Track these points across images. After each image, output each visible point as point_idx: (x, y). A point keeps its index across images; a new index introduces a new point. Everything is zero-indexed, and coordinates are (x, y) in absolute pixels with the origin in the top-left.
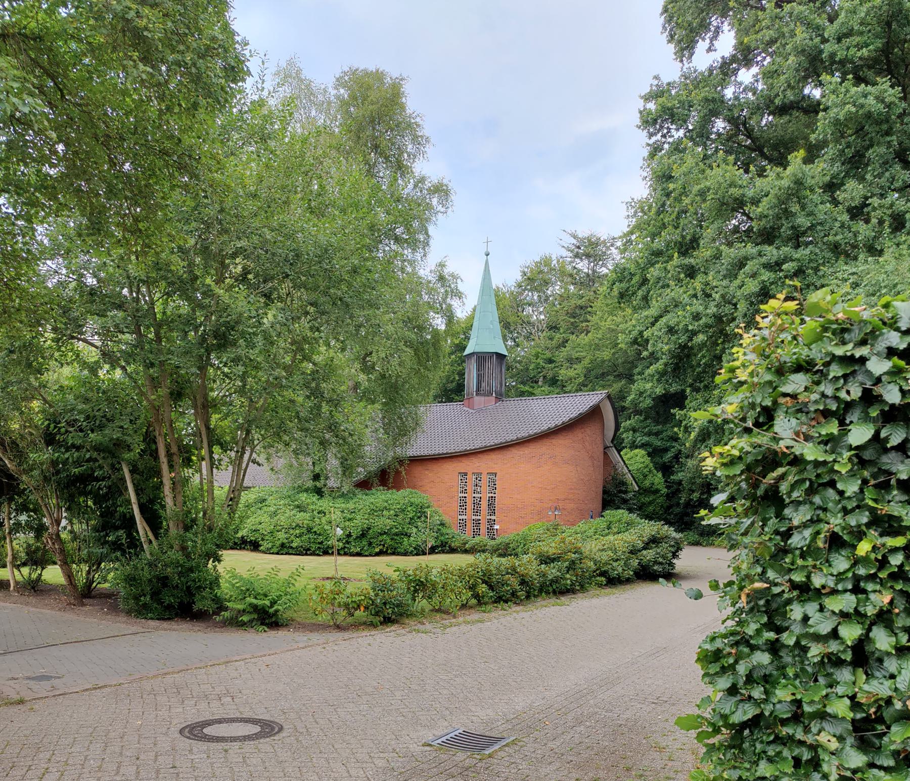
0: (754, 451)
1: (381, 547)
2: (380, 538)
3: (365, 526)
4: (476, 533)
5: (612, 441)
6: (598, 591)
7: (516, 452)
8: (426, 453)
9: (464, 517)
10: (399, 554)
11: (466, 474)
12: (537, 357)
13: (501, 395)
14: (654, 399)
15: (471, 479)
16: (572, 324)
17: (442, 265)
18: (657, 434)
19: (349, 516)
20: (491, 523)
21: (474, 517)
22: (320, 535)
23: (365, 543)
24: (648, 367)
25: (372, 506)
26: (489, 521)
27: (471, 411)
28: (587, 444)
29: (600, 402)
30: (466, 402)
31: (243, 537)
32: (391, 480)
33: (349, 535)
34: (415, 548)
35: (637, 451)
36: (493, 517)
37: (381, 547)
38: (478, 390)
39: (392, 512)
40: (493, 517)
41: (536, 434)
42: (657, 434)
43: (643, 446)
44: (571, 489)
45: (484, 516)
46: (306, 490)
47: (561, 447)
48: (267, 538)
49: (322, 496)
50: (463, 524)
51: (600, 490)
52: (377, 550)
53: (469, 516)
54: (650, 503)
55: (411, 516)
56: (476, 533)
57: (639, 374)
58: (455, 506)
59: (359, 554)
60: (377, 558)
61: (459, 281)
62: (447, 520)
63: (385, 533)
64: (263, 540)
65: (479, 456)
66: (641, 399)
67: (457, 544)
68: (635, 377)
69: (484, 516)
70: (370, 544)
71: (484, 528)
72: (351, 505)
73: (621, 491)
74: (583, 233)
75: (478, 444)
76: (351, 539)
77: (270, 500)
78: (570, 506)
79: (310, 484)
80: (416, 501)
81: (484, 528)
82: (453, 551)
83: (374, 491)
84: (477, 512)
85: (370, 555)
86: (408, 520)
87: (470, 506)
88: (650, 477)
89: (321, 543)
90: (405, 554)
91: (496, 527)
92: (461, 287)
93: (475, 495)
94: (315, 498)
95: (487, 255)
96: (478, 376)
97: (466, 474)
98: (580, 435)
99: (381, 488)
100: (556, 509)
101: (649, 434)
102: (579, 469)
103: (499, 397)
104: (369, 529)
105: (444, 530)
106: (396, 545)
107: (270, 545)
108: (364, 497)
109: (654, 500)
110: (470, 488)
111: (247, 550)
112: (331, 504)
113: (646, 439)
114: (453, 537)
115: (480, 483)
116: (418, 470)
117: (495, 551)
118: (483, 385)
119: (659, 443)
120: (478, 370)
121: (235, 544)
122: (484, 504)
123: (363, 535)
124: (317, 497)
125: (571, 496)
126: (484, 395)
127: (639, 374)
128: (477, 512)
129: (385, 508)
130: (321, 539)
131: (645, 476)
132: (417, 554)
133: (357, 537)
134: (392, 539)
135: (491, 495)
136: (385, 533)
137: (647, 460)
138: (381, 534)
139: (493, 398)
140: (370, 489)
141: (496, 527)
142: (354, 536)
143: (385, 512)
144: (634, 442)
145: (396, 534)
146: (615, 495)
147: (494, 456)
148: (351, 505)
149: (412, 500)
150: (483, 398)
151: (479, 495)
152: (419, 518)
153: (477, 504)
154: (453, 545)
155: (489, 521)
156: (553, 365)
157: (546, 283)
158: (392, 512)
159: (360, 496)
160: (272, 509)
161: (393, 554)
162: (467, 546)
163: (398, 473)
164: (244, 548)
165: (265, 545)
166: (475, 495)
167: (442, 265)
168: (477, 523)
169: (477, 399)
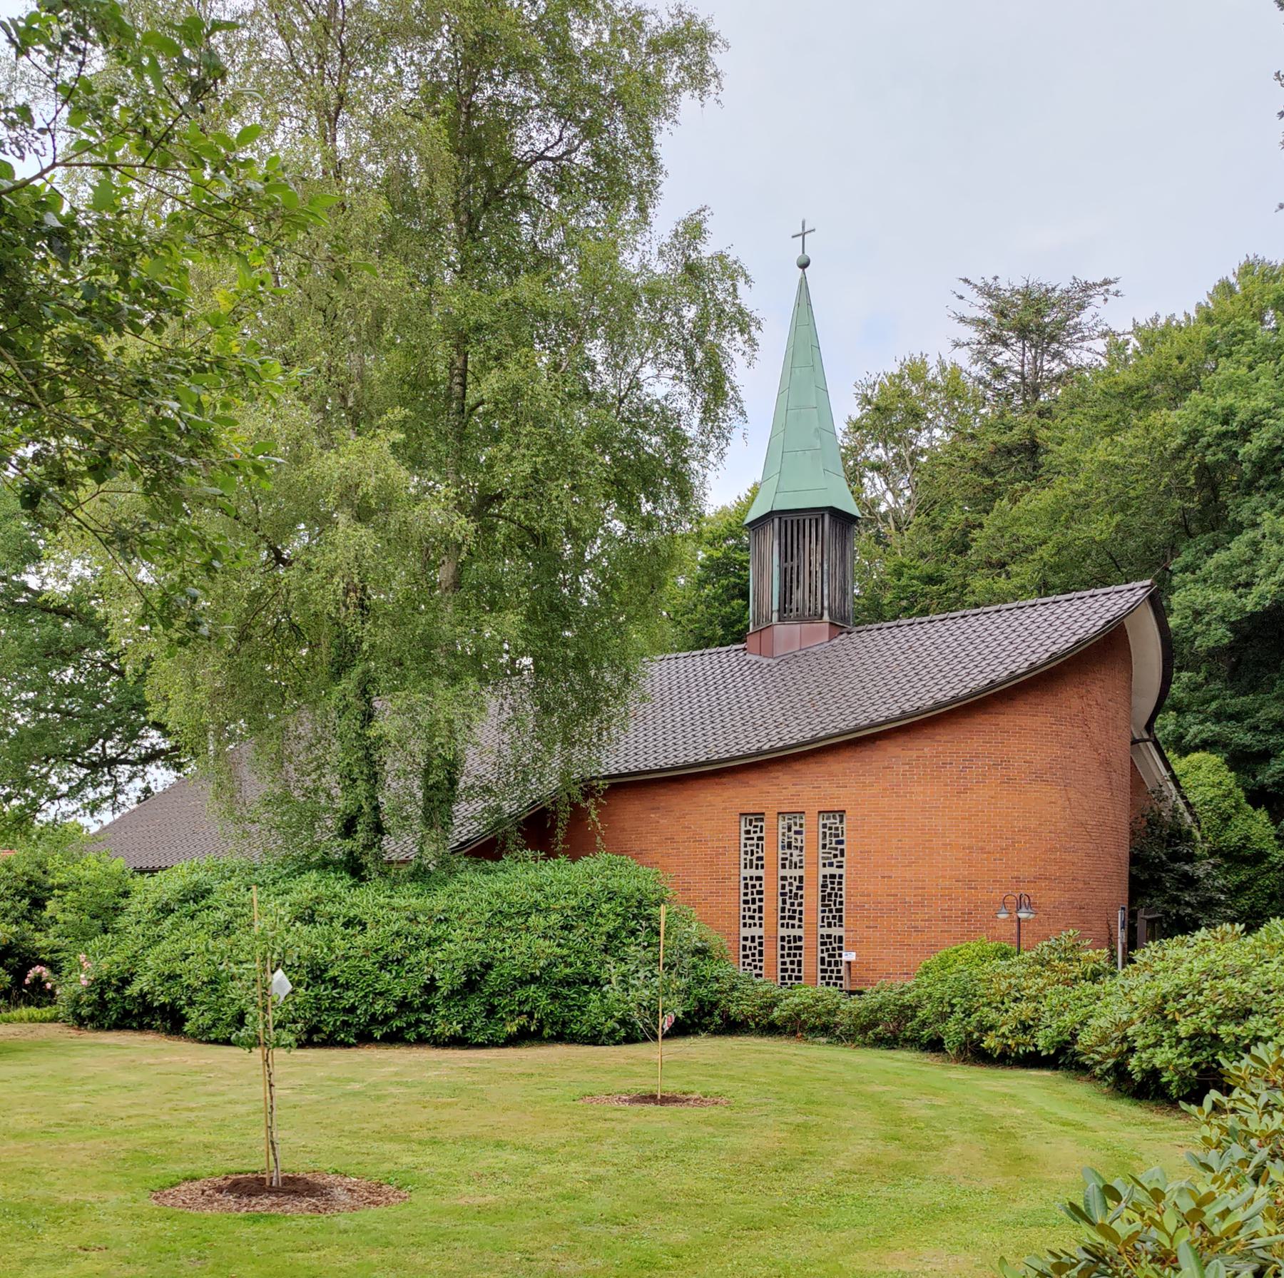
1: (523, 1020)
2: (520, 994)
3: (476, 959)
4: (791, 975)
7: (896, 755)
8: (651, 765)
9: (756, 931)
10: (574, 1039)
11: (760, 816)
12: (899, 574)
13: (844, 619)
14: (1234, 627)
15: (775, 829)
16: (986, 489)
17: (693, 230)
18: (1237, 717)
19: (429, 931)
20: (832, 946)
21: (783, 932)
22: (347, 987)
23: (475, 1006)
24: (1209, 553)
25: (497, 903)
26: (825, 940)
27: (765, 661)
28: (1094, 726)
29: (1131, 610)
30: (752, 641)
31: (143, 995)
32: (560, 835)
33: (431, 987)
34: (622, 1022)
35: (1196, 757)
36: (835, 931)
37: (523, 1020)
38: (785, 612)
39: (554, 918)
40: (835, 931)
41: (955, 699)
42: (1237, 717)
43: (1206, 745)
45: (812, 927)
46: (324, 865)
47: (1071, 700)
48: (199, 997)
49: (363, 879)
50: (753, 951)
51: (1125, 854)
52: (512, 1028)
53: (770, 928)
55: (609, 927)
56: (791, 975)
57: (1185, 569)
58: (733, 902)
59: (458, 1042)
60: (510, 1053)
61: (741, 283)
62: (715, 939)
63: (534, 979)
64: (191, 1003)
65: (797, 766)
66: (1198, 628)
67: (746, 1008)
68: (1176, 580)
69: (812, 927)
70: (491, 1011)
71: (811, 960)
72: (439, 901)
73: (1175, 857)
74: (1012, 278)
75: (795, 733)
76: (436, 999)
77: (222, 892)
78: (1049, 897)
79: (339, 849)
80: (627, 885)
81: (811, 960)
82: (732, 1027)
83: (507, 861)
84: (792, 916)
85: (491, 1044)
86: (600, 941)
87: (771, 903)
88: (1238, 821)
89: (352, 1010)
90: (594, 1039)
91: (849, 956)
92: (748, 298)
93: (787, 872)
94: (339, 884)
95: (804, 265)
96: (784, 573)
97: (760, 816)
98: (1076, 702)
99: (529, 853)
101: (1219, 717)
102: (1072, 795)
103: (840, 625)
104: (489, 967)
105: (708, 969)
106: (567, 1014)
107: (207, 1019)
108: (479, 879)
109: (1252, 880)
110: (773, 853)
111: (157, 1030)
112: (382, 900)
113: (1211, 729)
114: (734, 988)
115: (797, 841)
116: (632, 811)
117: (864, 1029)
118: (797, 595)
119: (1247, 739)
120: (786, 555)
121: (127, 1014)
122: (811, 898)
123: (471, 985)
124: (348, 881)
126: (801, 619)
127: (1185, 569)
128: (792, 916)
129: (536, 905)
130: (350, 997)
131: (1226, 819)
132: (630, 1040)
133: (453, 992)
134: (554, 997)
135: (828, 871)
136: (534, 979)
137: (1229, 778)
138: (523, 983)
139: (824, 626)
140: (498, 858)
141: (849, 956)
142: (445, 990)
143: (533, 919)
144: (1182, 737)
145: (567, 982)
146: (1161, 866)
147: (836, 766)
148: (439, 901)
149: (614, 884)
150: (797, 628)
151: (797, 873)
152: (633, 933)
153: (791, 895)
154: (734, 1009)
155: (825, 940)
156: (943, 587)
157: (916, 416)
158: (554, 918)
159: (466, 877)
160: (220, 916)
161: (559, 1038)
162: (776, 1013)
163: (578, 814)
164: (150, 1027)
165: (196, 1018)
166: (787, 872)
167: (693, 230)
168: (793, 946)
169: (782, 631)
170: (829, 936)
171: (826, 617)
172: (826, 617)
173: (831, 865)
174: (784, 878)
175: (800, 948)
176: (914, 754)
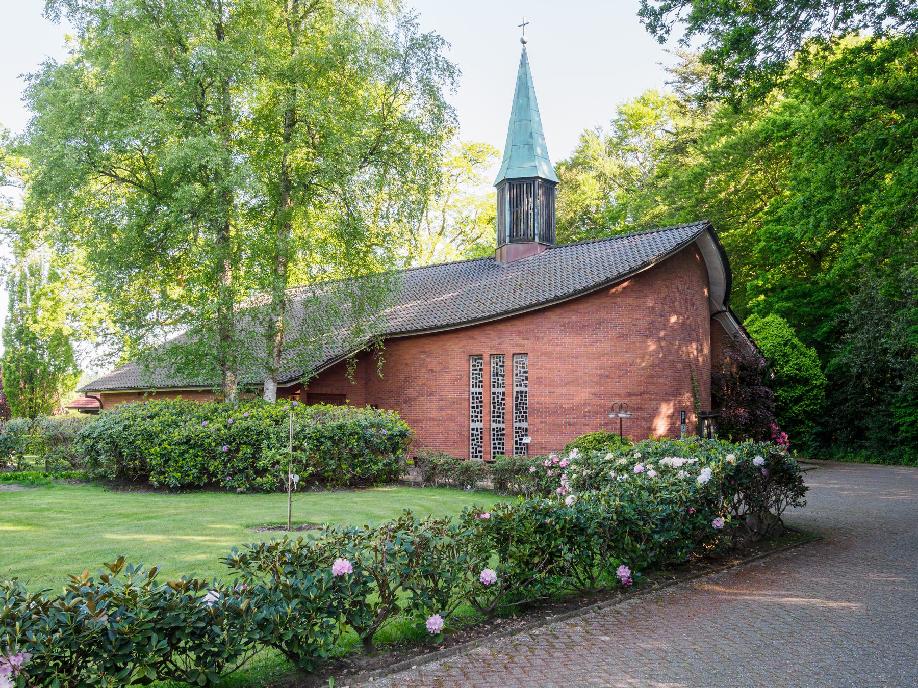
0: (702, 124)
5: (726, 302)
6: (342, 489)
11: (480, 357)
21: (494, 425)
36: (524, 425)
38: (511, 236)
40: (524, 425)
44: (652, 377)
54: (797, 400)
84: (499, 416)
87: (487, 408)
91: (527, 440)
93: (496, 390)
97: (480, 357)
100: (621, 407)
116: (410, 352)
122: (510, 404)
125: (652, 388)
126: (522, 241)
135: (519, 389)
151: (502, 390)
166: (496, 390)
168: (500, 434)
170: (520, 428)
171: (537, 240)
172: (537, 240)
173: (521, 385)
174: (494, 393)
175: (503, 435)
176: (566, 320)
